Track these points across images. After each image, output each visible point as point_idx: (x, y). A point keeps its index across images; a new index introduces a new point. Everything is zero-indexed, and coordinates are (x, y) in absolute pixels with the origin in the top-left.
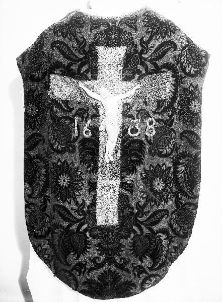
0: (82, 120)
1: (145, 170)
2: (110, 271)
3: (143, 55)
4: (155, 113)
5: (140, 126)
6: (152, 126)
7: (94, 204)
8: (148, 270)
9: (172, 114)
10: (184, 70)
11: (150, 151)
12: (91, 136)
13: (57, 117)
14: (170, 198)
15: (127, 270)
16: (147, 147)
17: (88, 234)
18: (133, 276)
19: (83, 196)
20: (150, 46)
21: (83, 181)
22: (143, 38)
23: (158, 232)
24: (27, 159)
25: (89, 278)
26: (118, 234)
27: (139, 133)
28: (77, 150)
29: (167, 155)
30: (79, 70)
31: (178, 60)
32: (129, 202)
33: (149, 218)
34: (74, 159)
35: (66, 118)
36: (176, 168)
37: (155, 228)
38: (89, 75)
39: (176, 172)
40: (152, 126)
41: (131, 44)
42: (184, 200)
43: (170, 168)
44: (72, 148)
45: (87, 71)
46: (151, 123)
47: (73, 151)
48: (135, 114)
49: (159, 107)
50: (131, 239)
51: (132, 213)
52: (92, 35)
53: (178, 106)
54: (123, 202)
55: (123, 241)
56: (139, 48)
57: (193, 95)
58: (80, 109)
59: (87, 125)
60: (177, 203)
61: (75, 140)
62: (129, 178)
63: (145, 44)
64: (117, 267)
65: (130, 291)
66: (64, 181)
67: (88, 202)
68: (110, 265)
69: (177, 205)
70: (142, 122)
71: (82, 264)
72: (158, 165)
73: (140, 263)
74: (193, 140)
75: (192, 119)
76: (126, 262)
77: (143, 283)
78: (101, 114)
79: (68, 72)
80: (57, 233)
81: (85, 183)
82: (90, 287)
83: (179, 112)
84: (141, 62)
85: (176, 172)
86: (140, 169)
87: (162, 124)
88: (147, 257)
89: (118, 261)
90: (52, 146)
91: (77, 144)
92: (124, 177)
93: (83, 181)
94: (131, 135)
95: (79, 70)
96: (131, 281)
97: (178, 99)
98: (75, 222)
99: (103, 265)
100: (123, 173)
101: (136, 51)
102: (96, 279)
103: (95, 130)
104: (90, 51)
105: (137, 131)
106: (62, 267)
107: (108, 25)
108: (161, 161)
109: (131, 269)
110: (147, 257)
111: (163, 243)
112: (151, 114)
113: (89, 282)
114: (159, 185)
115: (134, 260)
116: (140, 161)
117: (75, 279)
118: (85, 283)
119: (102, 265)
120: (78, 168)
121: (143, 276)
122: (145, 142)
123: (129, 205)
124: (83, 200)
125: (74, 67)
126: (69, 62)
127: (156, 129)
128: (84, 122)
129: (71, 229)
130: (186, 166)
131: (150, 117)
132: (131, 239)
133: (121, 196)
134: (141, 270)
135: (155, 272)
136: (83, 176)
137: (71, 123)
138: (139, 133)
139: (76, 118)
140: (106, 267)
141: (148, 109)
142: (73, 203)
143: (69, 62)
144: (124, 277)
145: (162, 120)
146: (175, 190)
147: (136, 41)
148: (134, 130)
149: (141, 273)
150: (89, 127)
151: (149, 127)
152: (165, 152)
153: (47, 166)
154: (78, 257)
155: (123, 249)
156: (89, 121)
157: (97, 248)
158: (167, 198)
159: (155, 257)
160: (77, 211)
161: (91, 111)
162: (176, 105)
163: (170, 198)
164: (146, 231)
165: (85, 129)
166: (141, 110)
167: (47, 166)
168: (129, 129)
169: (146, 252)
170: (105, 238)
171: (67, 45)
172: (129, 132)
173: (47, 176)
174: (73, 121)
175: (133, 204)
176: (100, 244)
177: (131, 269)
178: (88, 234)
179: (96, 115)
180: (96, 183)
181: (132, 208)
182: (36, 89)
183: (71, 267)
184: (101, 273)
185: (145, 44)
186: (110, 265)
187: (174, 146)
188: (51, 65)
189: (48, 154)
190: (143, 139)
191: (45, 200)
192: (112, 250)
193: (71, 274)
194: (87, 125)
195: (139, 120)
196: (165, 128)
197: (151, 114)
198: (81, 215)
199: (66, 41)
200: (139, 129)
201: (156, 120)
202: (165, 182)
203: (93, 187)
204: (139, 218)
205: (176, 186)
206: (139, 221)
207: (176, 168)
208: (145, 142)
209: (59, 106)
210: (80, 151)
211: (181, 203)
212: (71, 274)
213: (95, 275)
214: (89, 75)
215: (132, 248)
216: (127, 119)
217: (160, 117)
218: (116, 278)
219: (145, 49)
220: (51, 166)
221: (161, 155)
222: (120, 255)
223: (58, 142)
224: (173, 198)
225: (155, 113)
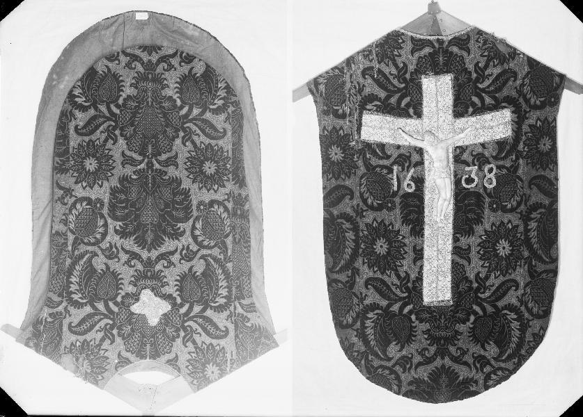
0: (403, 170)
1: (486, 231)
2: (443, 366)
3: (111, 322)
4: (496, 158)
5: (477, 175)
6: (492, 175)
7: (420, 279)
8: (493, 362)
9: (517, 158)
10: (527, 101)
11: (102, 205)
12: (415, 190)
13: (371, 165)
14: (521, 266)
15: (466, 364)
16: (487, 200)
17: (413, 317)
18: (474, 371)
19: (406, 265)
20: (102, 334)
21: (405, 248)
22: (478, 62)
23: (89, 107)
24: (328, 218)
25: (416, 376)
26: (453, 317)
27: (475, 183)
28: (194, 208)
29: (512, 210)
30: (399, 101)
31: (520, 91)
32: (127, 143)
33: (494, 292)
34: (394, 218)
35: (383, 167)
36: (526, 225)
37: (92, 112)
38: (411, 111)
39: (527, 231)
40: (492, 175)
41: (463, 70)
42: (540, 267)
43: (517, 226)
44: (204, 206)
45: (408, 105)
46: (491, 171)
47: (201, 203)
48: (470, 159)
49: (500, 151)
50: (472, 324)
51: (470, 288)
52: (174, 349)
53: (524, 148)
54: (457, 269)
55: (462, 328)
56: (474, 75)
57: (549, 130)
58: (400, 156)
59: (410, 174)
60: (532, 273)
61: (395, 194)
62: (464, 241)
63: (481, 73)
64: (452, 360)
65: (469, 388)
66: (381, 247)
67: (413, 276)
68: (150, 61)
69: (531, 275)
70: (480, 169)
71: (186, 63)
72: (502, 222)
73: (110, 65)
74: (550, 188)
75: (549, 159)
76: (128, 65)
77: (488, 377)
78: (426, 163)
79: (386, 108)
80: (370, 319)
81: (409, 249)
82: (418, 387)
83: (526, 155)
84: (476, 92)
85: (527, 231)
86: (479, 229)
87: (505, 171)
88: (491, 342)
89: (140, 66)
90: (365, 201)
91: (195, 213)
92: (458, 240)
93: (405, 248)
94: (464, 185)
95: (399, 101)
96: (473, 378)
97: (524, 138)
98: (396, 301)
99: (435, 360)
100: (458, 235)
101: (470, 79)
102: (426, 379)
103: (419, 181)
104: (412, 80)
105: (473, 181)
106: (376, 363)
107: (433, 47)
108: (506, 217)
109: (471, 361)
110: (491, 342)
111: (513, 326)
112: (491, 159)
113: (417, 382)
114: (504, 248)
115: (475, 349)
116: (479, 220)
117: (398, 378)
118: (410, 383)
119: (159, 62)
120: (399, 230)
121: (487, 369)
122: (485, 195)
123: (467, 278)
124: (406, 272)
125: (393, 100)
126: (205, 314)
127: (497, 177)
128: (405, 173)
129: (391, 309)
130: (538, 221)
131: (490, 163)
132: (472, 324)
133: (455, 265)
134: (482, 361)
135: (503, 365)
136: (406, 241)
137: (388, 173)
138: (475, 183)
139: (395, 168)
140: (438, 362)
141: (486, 154)
142: (393, 276)
143: (205, 314)
144: (463, 373)
145: (503, 167)
146: (526, 254)
147: (471, 67)
148: (469, 181)
149: (485, 366)
150: (413, 179)
151: (489, 176)
152: (84, 204)
153: (356, 229)
154: (402, 347)
155: (459, 337)
156: (412, 170)
157: (426, 336)
158: (516, 266)
159: (502, 343)
160: (400, 287)
161: (412, 159)
162: (521, 146)
163: (521, 266)
164: (103, 108)
165: (407, 181)
166: (478, 154)
167: (356, 229)
168: (464, 178)
169: (105, 77)
170: (436, 322)
171: (208, 333)
172: (463, 182)
173: (356, 241)
174: (391, 171)
175: (472, 277)
176: (429, 330)
177: (471, 361)
178: (413, 317)
179: (421, 163)
180: (422, 249)
181: (471, 282)
182: (341, 128)
183: (393, 362)
184: (433, 371)
185: (481, 73)
186: (443, 358)
187: (522, 197)
188: (229, 308)
189: (360, 213)
190: (481, 191)
191: (353, 274)
192: (446, 339)
193: (392, 372)
194: (410, 174)
195: (476, 167)
196: (508, 179)
197: (491, 159)
198: (188, 127)
199: (208, 340)
200: (476, 179)
201: (498, 167)
202: (511, 244)
203: (419, 254)
204: (479, 295)
205: (528, 249)
206: (480, 298)
207: (526, 225)
208: (485, 195)
209: (374, 153)
210: (192, 205)
211: (536, 271)
212: (392, 372)
213: (423, 373)
214: (411, 111)
215: (121, 84)
216: (462, 166)
217: (501, 163)
218: (452, 375)
219: (482, 77)
220: (362, 226)
221: (505, 210)
222: (455, 345)
223: (218, 214)
224: (524, 265)
225: (496, 158)
